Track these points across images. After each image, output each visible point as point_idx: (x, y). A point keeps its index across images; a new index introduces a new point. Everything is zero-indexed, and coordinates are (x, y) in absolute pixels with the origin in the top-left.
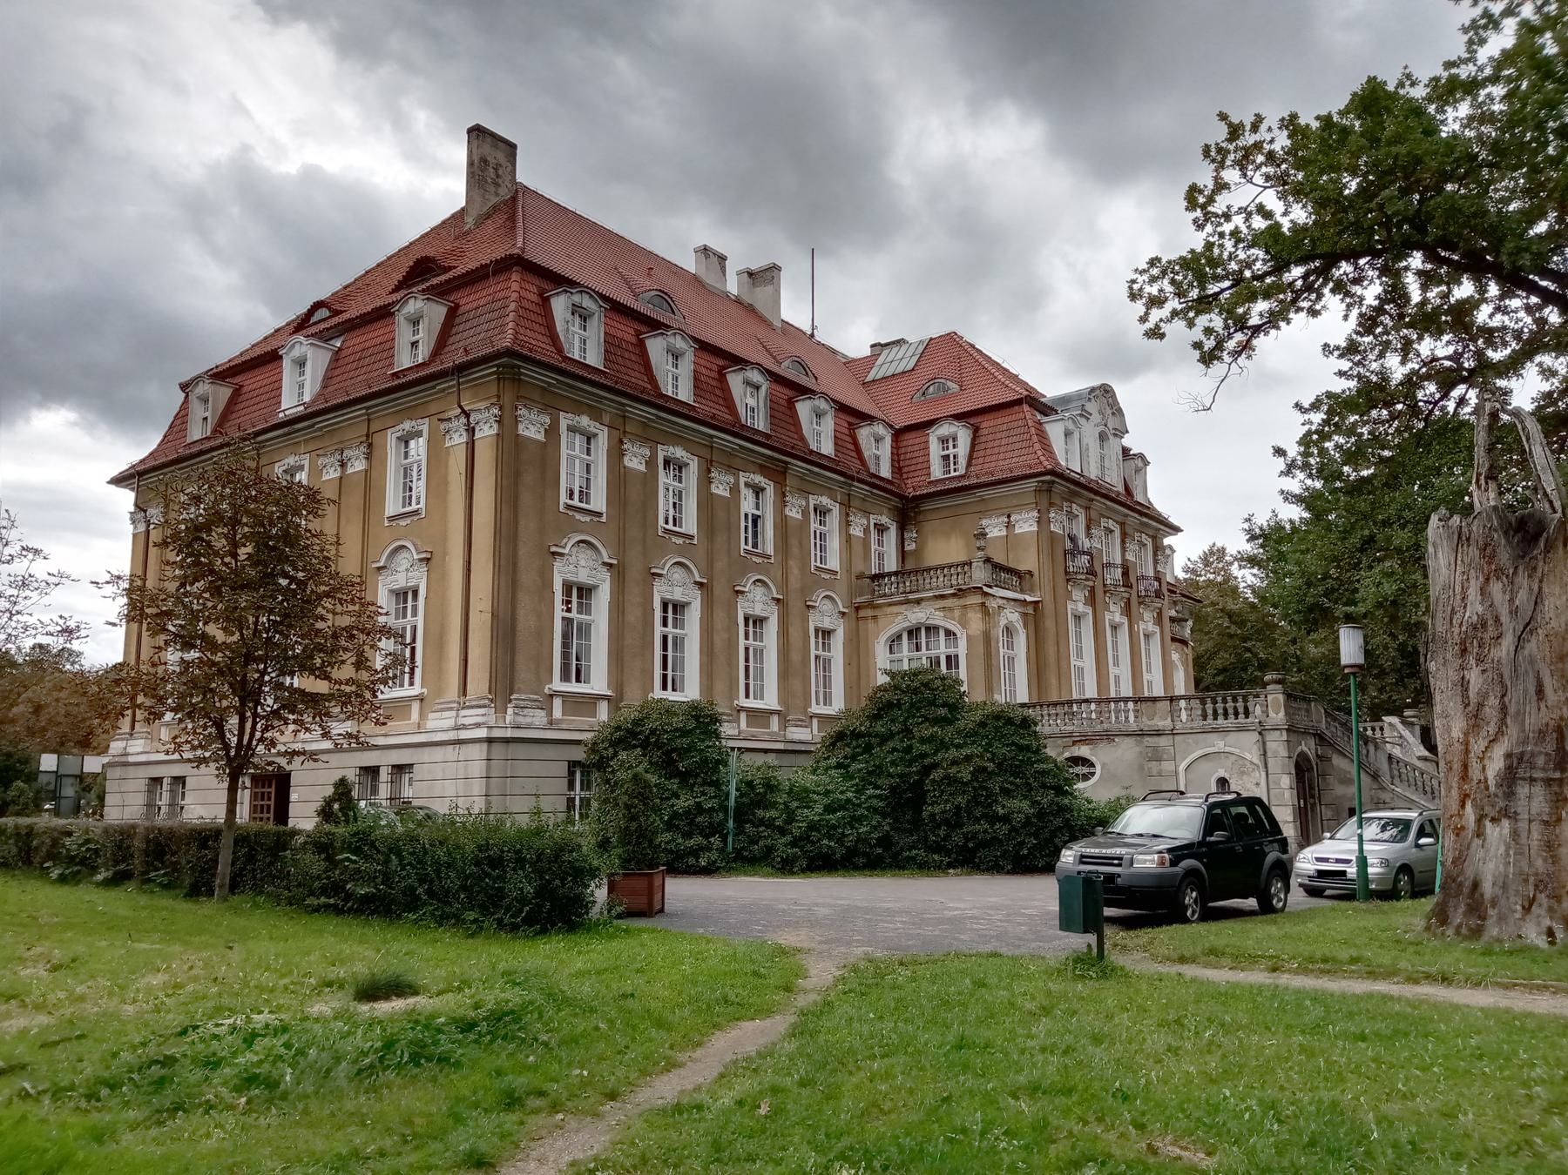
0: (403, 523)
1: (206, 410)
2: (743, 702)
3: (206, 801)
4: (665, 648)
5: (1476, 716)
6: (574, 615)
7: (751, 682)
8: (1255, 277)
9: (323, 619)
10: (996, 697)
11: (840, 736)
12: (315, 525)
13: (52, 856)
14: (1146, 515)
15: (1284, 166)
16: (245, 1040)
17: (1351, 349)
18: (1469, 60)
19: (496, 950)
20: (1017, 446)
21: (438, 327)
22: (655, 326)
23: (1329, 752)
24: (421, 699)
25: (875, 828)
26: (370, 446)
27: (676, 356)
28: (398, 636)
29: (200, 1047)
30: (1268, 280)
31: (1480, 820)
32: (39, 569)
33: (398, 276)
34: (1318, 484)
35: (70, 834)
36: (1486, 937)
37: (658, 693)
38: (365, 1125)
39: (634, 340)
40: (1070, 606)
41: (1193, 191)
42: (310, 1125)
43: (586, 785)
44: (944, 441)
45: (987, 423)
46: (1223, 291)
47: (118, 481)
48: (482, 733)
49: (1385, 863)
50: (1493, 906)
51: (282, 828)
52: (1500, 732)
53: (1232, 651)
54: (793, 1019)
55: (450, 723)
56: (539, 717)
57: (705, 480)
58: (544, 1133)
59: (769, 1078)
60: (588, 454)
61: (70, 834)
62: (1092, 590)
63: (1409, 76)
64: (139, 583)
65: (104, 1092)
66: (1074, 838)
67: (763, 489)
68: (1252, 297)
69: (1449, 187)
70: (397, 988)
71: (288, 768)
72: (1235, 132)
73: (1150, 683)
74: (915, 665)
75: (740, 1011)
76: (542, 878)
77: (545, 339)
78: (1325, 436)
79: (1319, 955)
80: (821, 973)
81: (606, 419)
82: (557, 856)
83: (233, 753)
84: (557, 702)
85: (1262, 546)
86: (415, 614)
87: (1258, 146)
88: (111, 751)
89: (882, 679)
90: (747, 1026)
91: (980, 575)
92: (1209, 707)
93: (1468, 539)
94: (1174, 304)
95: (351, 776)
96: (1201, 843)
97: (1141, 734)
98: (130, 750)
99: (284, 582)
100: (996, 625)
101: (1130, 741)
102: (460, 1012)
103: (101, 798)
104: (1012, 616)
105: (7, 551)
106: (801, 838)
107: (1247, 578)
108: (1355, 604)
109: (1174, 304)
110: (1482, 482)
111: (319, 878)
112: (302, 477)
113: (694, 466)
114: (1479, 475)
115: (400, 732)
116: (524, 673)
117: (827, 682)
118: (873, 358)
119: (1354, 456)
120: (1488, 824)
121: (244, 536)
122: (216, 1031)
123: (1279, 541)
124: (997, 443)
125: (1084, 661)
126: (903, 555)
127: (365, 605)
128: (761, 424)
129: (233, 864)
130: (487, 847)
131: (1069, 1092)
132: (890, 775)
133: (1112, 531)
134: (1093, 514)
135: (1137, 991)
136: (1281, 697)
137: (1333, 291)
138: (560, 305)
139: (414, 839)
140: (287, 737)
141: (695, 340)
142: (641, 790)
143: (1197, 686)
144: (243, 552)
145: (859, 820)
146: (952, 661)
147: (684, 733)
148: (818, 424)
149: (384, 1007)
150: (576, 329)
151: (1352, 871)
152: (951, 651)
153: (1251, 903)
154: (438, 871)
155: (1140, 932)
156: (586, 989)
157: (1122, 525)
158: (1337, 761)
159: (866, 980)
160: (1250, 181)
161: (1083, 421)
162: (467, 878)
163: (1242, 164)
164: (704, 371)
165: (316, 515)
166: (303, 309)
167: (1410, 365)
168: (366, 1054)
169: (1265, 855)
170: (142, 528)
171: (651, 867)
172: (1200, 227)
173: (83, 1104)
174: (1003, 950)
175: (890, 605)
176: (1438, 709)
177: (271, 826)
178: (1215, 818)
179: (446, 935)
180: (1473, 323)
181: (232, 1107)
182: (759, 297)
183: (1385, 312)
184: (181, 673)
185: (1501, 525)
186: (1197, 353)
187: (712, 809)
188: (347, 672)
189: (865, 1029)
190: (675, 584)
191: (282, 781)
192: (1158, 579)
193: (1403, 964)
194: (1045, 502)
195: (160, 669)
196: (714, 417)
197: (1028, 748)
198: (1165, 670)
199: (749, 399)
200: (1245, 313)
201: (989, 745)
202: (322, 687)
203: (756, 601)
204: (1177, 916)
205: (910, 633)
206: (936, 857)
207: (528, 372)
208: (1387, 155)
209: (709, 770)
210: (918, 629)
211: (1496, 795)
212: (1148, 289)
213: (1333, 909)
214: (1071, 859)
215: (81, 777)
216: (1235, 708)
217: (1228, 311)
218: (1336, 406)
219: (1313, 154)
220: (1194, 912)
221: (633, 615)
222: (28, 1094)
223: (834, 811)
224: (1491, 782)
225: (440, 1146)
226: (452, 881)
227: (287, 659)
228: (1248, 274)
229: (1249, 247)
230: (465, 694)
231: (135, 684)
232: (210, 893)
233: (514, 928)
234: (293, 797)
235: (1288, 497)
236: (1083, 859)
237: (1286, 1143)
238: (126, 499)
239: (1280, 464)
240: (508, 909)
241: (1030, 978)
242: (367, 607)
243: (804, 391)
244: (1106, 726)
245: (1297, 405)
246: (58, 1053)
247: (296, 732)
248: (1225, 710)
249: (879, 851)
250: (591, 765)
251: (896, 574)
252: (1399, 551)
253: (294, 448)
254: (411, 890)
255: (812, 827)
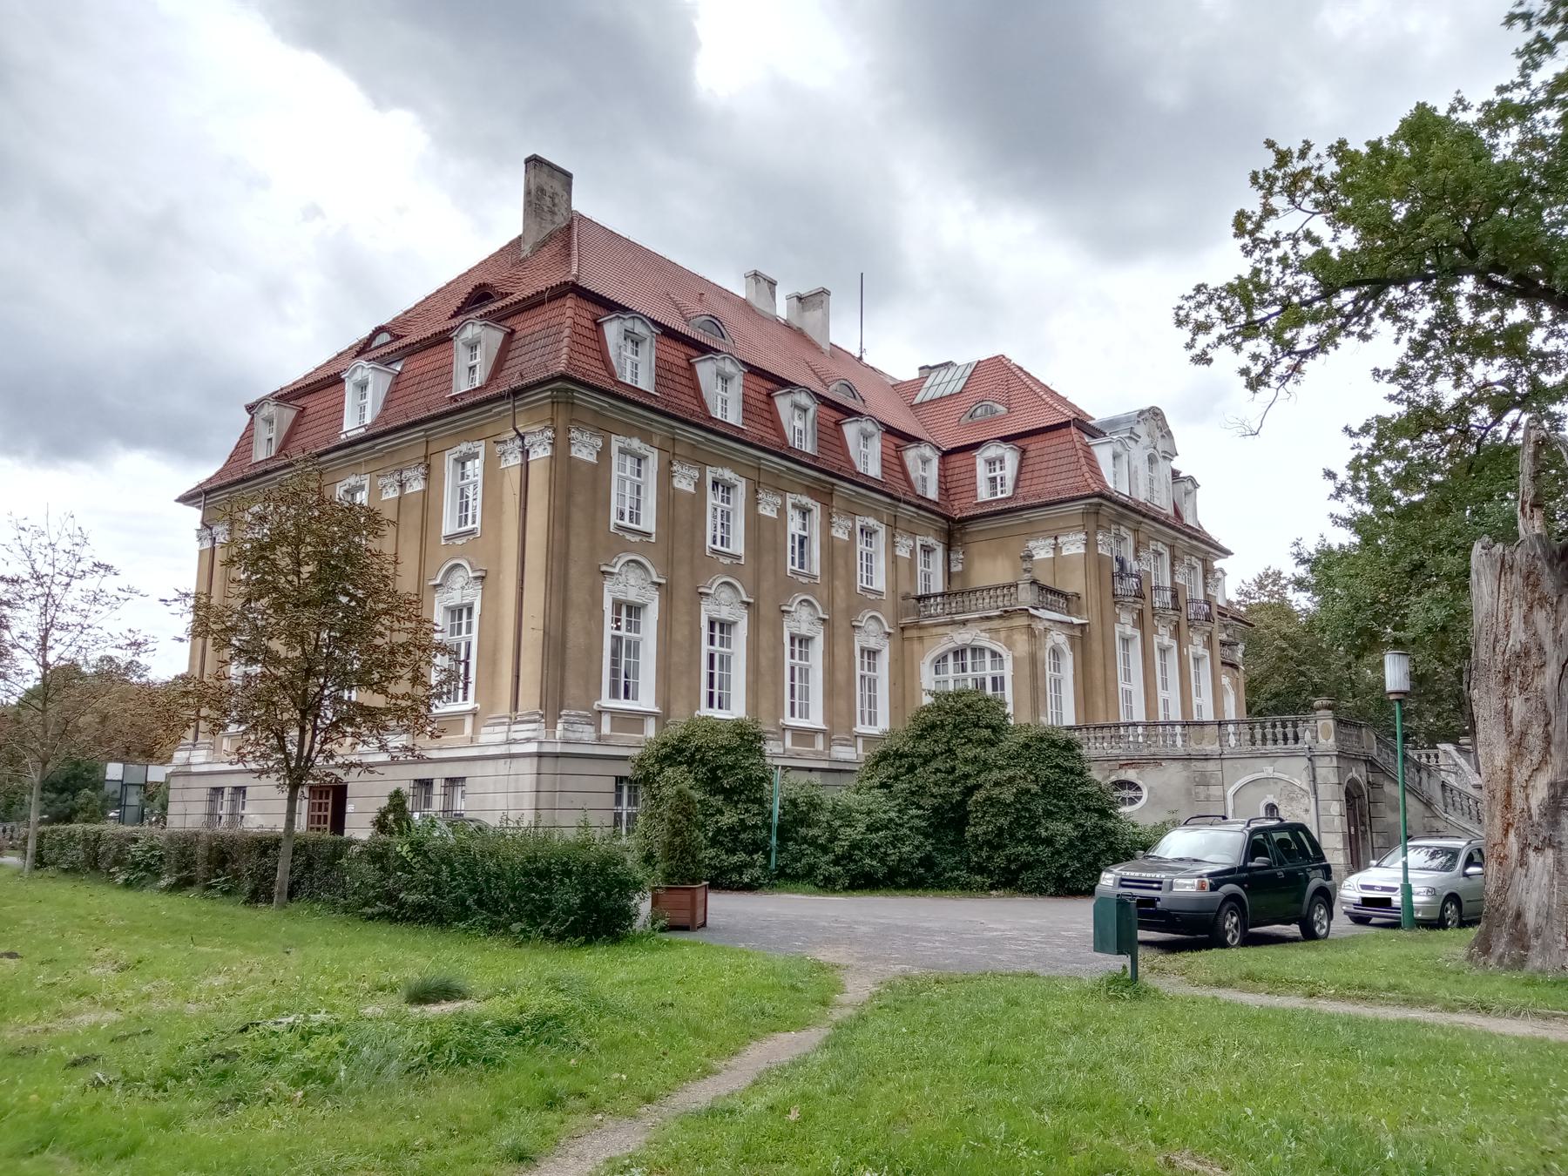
0: (459, 542)
1: (271, 431)
2: (789, 721)
3: (266, 811)
4: (712, 666)
5: (1519, 745)
6: (623, 633)
7: (797, 701)
8: (1304, 303)
9: (382, 635)
10: (1042, 719)
11: (884, 757)
12: (374, 545)
13: (117, 862)
14: (1196, 538)
15: (1333, 192)
16: (302, 1038)
17: (1402, 372)
18: (1522, 84)
19: (542, 959)
20: (1064, 468)
21: (494, 352)
22: (704, 349)
23: (1380, 778)
24: (474, 713)
25: (917, 848)
26: (428, 466)
27: (726, 379)
28: (450, 651)
29: (260, 1043)
30: (1317, 305)
31: (1522, 850)
32: (110, 584)
33: (456, 303)
34: (1368, 509)
35: (135, 840)
36: (1529, 968)
37: (704, 711)
38: (413, 1119)
39: (684, 364)
40: (1118, 628)
41: (1241, 219)
42: (362, 1119)
43: (633, 801)
44: (991, 463)
45: (1034, 445)
46: (1270, 316)
47: (186, 499)
48: (532, 748)
49: (1432, 891)
50: (1537, 937)
51: (338, 837)
52: (1544, 761)
53: (1287, 673)
54: (828, 1032)
55: (501, 737)
56: (588, 733)
57: (753, 502)
58: (583, 1131)
59: (800, 1086)
60: (639, 475)
61: (135, 840)
62: (1141, 613)
63: (1460, 101)
64: (204, 600)
65: (170, 1083)
66: (1116, 861)
67: (810, 511)
68: (1299, 322)
69: (1503, 211)
70: (445, 992)
71: (345, 779)
72: (1283, 158)
73: (1199, 707)
74: (960, 685)
75: (777, 1023)
76: (587, 890)
77: (598, 364)
78: (1374, 461)
79: (1356, 982)
80: (857, 990)
81: (656, 441)
82: (602, 870)
83: (293, 764)
84: (606, 719)
85: (1312, 571)
86: (469, 631)
87: (1306, 172)
88: (175, 761)
89: (927, 700)
90: (783, 1037)
91: (1026, 596)
92: (1258, 732)
93: (1511, 567)
94: (1221, 329)
95: (406, 788)
96: (1242, 869)
97: (1189, 758)
98: (192, 760)
99: (344, 600)
100: (1042, 647)
101: (1177, 766)
102: (505, 1016)
103: (164, 807)
104: (1059, 638)
105: (80, 567)
106: (843, 857)
107: (1302, 601)
108: (1404, 629)
109: (1221, 329)
110: (1528, 509)
111: (373, 887)
112: (362, 498)
113: (742, 486)
114: (1524, 503)
115: (453, 746)
116: (573, 690)
117: (872, 702)
118: (922, 379)
119: (1405, 481)
120: (1531, 854)
121: (307, 555)
122: (274, 1028)
123: (1328, 567)
124: (1044, 465)
125: (1132, 684)
126: (949, 576)
127: (421, 621)
128: (809, 447)
129: (291, 872)
130: (535, 859)
131: (1093, 1106)
132: (932, 795)
133: (1160, 554)
134: (1142, 537)
135: (1170, 1013)
136: (1331, 723)
137: (1382, 316)
138: (613, 331)
139: (465, 850)
140: (345, 749)
141: (744, 363)
142: (684, 805)
143: (1249, 711)
144: (306, 570)
145: (902, 840)
146: (997, 682)
147: (729, 750)
148: (866, 446)
149: (433, 1010)
150: (628, 353)
151: (1397, 899)
152: (997, 672)
153: (1294, 930)
154: (487, 881)
155: (1179, 956)
156: (627, 998)
157: (1172, 547)
158: (1389, 788)
159: (902, 997)
160: (1299, 207)
161: (1131, 443)
162: (515, 889)
163: (1292, 190)
164: (752, 394)
165: (376, 535)
166: (365, 332)
167: (1462, 390)
168: (416, 1053)
169: (1308, 880)
170: (207, 545)
171: (694, 881)
172: (1249, 253)
173: (152, 1095)
174: (1040, 971)
175: (936, 625)
176: (1481, 737)
177: (328, 836)
178: (1255, 847)
179: (494, 944)
180: (1527, 348)
181: (289, 1100)
182: (809, 321)
183: (1435, 337)
184: (245, 687)
185: (1544, 553)
186: (1243, 380)
187: (755, 826)
188: (403, 687)
189: (897, 1043)
190: (722, 604)
191: (339, 794)
192: (1208, 603)
193: (1442, 992)
194: (1092, 526)
195: (225, 683)
196: (762, 439)
197: (1072, 771)
198: (1215, 696)
199: (797, 422)
200: (1293, 339)
201: (1033, 767)
202: (378, 701)
203: (802, 620)
204: (1216, 940)
205: (956, 653)
206: (978, 878)
207: (581, 395)
208: (1435, 180)
209: (750, 789)
210: (963, 651)
211: (1540, 825)
212: (1194, 315)
213: (1377, 937)
214: (1111, 883)
215: (145, 786)
216: (1274, 734)
217: (1277, 336)
218: (1385, 430)
219: (1359, 180)
220: (1234, 937)
221: (681, 633)
222: (101, 1084)
223: (877, 830)
224: (1535, 811)
225: (485, 1141)
226: (500, 892)
227: (345, 674)
228: (1295, 299)
229: (1297, 273)
230: (516, 709)
231: (201, 697)
232: (269, 899)
233: (560, 938)
234: (350, 808)
235: (1337, 521)
236: (1123, 882)
237: (1303, 1161)
238: (193, 516)
239: (1330, 487)
240: (555, 920)
241: (1063, 998)
242: (423, 624)
243: (850, 413)
244: (1153, 750)
245: (1346, 429)
246: (128, 1047)
247: (353, 745)
248: (1264, 736)
249: (922, 871)
250: (637, 782)
251: (942, 595)
252: (1448, 577)
253: (355, 468)
254: (461, 902)
255: (855, 846)
